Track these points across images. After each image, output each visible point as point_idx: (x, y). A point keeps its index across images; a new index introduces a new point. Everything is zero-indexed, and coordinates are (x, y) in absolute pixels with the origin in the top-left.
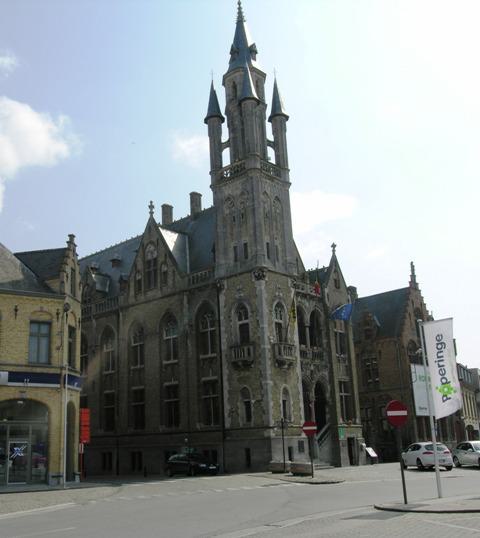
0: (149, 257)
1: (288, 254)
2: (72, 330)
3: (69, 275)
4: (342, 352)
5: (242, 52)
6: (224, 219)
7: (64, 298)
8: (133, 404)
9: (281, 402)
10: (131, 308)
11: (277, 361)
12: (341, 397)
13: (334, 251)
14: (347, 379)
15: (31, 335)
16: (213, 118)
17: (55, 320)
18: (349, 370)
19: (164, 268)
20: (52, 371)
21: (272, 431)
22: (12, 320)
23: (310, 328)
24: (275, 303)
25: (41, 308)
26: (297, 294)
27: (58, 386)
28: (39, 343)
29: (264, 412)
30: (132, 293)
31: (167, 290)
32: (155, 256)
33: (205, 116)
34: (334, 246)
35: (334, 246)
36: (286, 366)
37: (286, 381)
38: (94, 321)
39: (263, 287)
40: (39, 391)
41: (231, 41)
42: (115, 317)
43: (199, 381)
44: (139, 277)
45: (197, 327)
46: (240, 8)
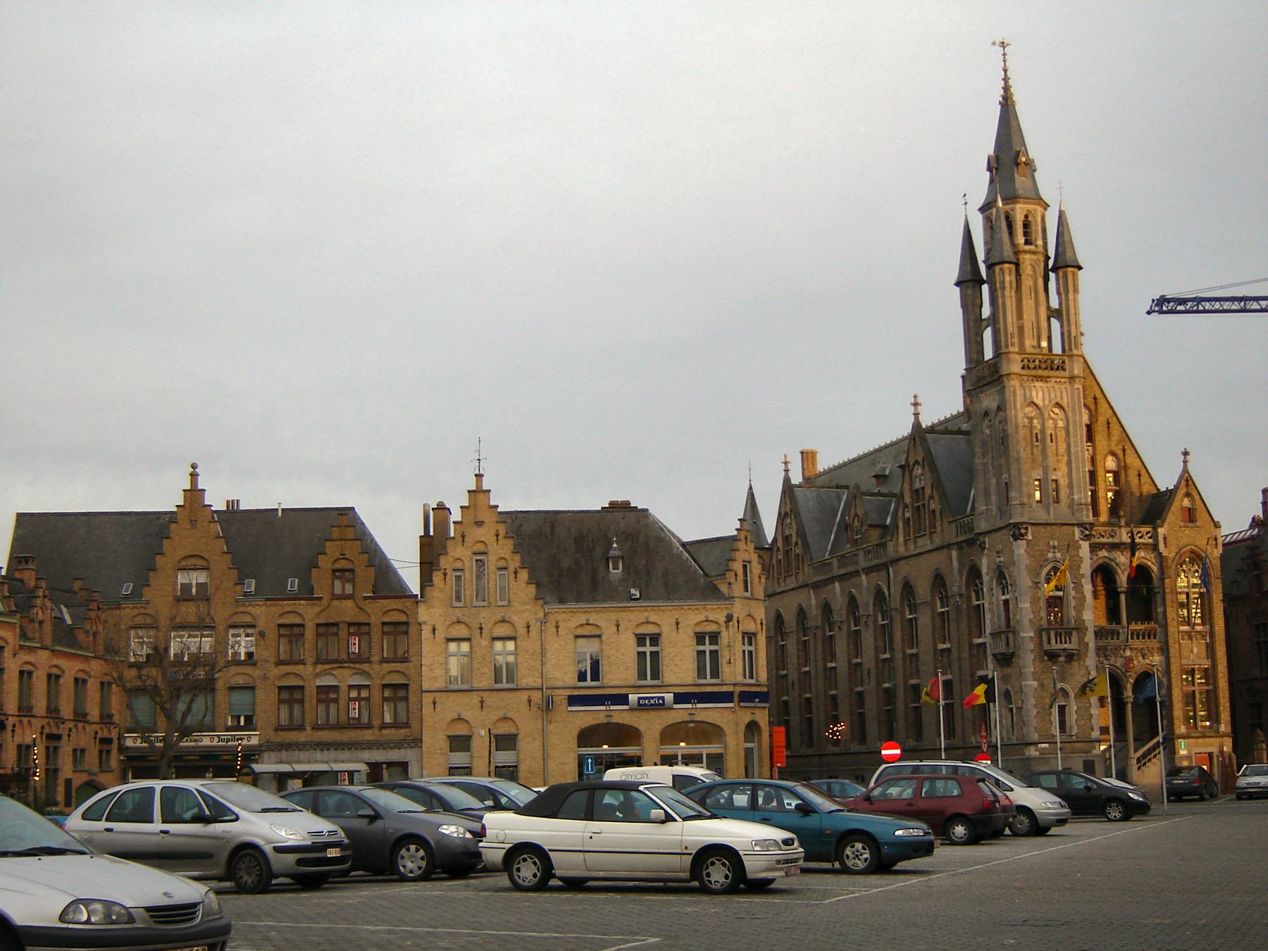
0: (917, 486)
1: (1075, 490)
4: (860, 695)
11: (1047, 653)
13: (1185, 462)
14: (1206, 664)
17: (723, 629)
18: (1211, 650)
19: (933, 506)
20: (724, 689)
21: (1032, 748)
22: (674, 634)
26: (1094, 548)
27: (731, 705)
30: (901, 539)
31: (938, 541)
33: (980, 204)
34: (1186, 454)
35: (1186, 454)
38: (864, 577)
39: (1022, 551)
40: (710, 712)
41: (987, 145)
43: (972, 675)
45: (969, 597)
46: (1006, 79)
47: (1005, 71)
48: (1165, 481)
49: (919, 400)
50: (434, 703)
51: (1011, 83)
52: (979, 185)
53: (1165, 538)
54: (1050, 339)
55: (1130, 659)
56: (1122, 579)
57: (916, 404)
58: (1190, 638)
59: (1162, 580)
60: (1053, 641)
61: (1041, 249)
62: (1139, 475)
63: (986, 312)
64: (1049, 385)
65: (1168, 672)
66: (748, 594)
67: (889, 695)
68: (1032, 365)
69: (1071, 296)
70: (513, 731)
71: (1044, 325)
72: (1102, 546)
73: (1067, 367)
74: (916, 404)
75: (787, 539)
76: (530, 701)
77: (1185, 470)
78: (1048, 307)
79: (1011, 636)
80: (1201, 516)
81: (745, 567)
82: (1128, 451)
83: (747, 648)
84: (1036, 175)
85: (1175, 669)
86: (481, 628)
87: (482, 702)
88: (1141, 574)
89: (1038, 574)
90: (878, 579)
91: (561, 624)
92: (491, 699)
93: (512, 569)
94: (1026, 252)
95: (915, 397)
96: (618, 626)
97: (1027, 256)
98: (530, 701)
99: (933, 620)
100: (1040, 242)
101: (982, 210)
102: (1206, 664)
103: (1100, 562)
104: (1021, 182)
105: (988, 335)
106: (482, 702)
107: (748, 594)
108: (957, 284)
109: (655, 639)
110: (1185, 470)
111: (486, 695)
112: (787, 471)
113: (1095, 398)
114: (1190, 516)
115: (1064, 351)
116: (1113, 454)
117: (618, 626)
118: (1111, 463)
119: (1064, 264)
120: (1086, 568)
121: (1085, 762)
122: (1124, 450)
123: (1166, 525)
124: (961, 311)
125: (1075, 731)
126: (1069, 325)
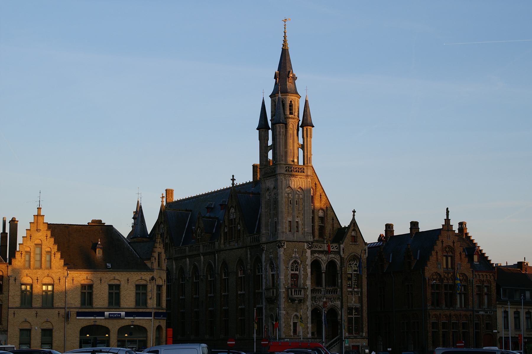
0: (231, 217)
1: (306, 227)
2: (159, 287)
3: (157, 258)
5: (284, 74)
7: (153, 271)
9: (292, 324)
11: (290, 299)
13: (354, 215)
15: (136, 293)
16: (263, 127)
17: (149, 283)
19: (239, 228)
20: (148, 310)
22: (126, 285)
24: (291, 262)
25: (141, 278)
26: (313, 253)
28: (215, 257)
30: (222, 241)
34: (354, 212)
35: (354, 212)
36: (296, 302)
37: (297, 311)
38: (202, 257)
39: (282, 253)
41: (275, 68)
44: (226, 230)
46: (285, 37)
47: (285, 33)
50: (14, 314)
51: (287, 38)
52: (270, 86)
53: (343, 249)
56: (324, 266)
60: (293, 294)
61: (296, 117)
62: (333, 219)
63: (270, 143)
64: (297, 179)
69: (309, 139)
70: (51, 327)
73: (305, 171)
76: (59, 314)
77: (354, 219)
81: (159, 255)
86: (37, 280)
87: (37, 314)
88: (331, 264)
89: (288, 264)
91: (75, 279)
92: (41, 312)
93: (53, 252)
95: (233, 176)
96: (101, 280)
98: (59, 314)
100: (296, 114)
104: (289, 85)
106: (37, 314)
109: (118, 287)
110: (354, 219)
111: (39, 310)
113: (316, 184)
115: (304, 164)
117: (101, 280)
120: (309, 262)
123: (344, 244)
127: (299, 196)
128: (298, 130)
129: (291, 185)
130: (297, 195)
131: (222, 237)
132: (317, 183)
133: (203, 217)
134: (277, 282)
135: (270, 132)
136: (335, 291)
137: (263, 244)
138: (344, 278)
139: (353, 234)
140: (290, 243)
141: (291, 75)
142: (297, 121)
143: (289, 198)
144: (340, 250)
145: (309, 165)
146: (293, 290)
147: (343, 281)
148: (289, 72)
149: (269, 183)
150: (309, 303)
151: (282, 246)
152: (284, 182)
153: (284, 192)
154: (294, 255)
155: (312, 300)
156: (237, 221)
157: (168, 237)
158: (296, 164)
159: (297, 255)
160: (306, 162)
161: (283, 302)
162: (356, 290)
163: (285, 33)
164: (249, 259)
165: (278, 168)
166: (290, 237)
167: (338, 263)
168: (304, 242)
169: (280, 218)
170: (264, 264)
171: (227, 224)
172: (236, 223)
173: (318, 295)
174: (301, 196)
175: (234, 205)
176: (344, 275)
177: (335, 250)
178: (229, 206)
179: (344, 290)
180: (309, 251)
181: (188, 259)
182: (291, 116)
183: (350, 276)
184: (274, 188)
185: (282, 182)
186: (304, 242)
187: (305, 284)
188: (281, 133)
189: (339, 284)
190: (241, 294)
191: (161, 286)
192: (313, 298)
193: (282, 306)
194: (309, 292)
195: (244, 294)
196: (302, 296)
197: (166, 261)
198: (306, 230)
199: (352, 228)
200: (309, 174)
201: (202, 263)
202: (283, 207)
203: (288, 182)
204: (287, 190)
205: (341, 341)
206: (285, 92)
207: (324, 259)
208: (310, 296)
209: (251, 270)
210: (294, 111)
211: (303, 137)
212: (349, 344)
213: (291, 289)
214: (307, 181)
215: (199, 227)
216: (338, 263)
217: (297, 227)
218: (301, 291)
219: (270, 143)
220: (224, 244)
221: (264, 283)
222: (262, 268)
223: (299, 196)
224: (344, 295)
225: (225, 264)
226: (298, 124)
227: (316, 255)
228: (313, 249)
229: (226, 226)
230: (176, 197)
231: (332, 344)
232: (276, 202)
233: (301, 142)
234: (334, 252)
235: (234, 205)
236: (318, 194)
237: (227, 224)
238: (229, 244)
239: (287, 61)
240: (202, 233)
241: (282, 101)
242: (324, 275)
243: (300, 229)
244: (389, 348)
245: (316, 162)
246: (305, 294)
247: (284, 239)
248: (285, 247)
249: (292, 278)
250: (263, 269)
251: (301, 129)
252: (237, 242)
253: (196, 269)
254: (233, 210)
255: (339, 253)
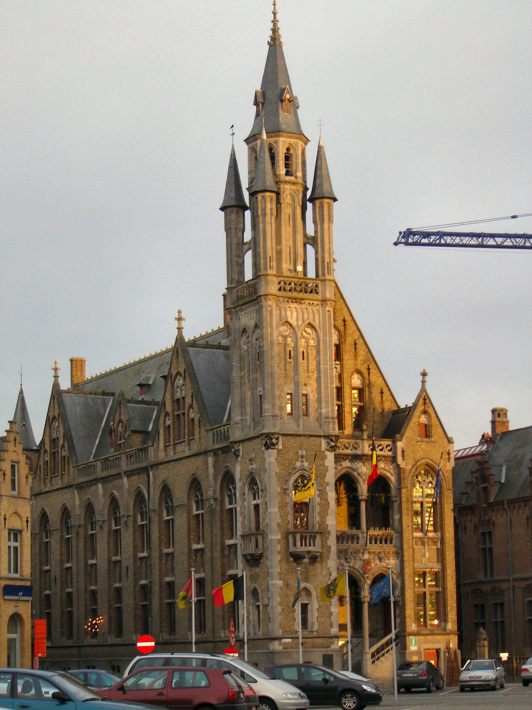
0: (178, 395)
1: (323, 405)
6: (241, 357)
8: (166, 601)
10: (161, 467)
11: (292, 555)
12: (9, 547)
13: (423, 382)
14: (437, 567)
16: (234, 206)
19: (192, 415)
23: (367, 501)
26: (339, 458)
28: (148, 476)
29: (269, 619)
30: (162, 445)
32: (183, 395)
33: (246, 136)
34: (424, 374)
35: (424, 374)
36: (306, 560)
38: (125, 479)
39: (273, 459)
42: (145, 476)
44: (168, 422)
45: (222, 501)
46: (275, 22)
47: (275, 14)
48: (405, 399)
49: (183, 315)
51: (279, 25)
52: (246, 119)
53: (403, 452)
54: (305, 264)
55: (368, 562)
56: (363, 489)
57: (179, 319)
58: (423, 543)
59: (399, 489)
61: (300, 180)
62: (382, 393)
63: (248, 236)
64: (304, 306)
65: (402, 574)
66: (15, 493)
67: (145, 591)
68: (288, 288)
69: (326, 225)
71: (300, 250)
72: (345, 457)
73: (320, 290)
74: (179, 319)
75: (54, 442)
77: (423, 390)
78: (305, 235)
79: (260, 538)
80: (436, 431)
81: (13, 467)
82: (373, 370)
83: (13, 544)
84: (299, 111)
85: (408, 572)
88: (379, 483)
89: (287, 481)
90: (138, 481)
94: (286, 182)
95: (179, 312)
97: (288, 186)
99: (189, 522)
100: (300, 174)
101: (247, 141)
102: (437, 567)
103: (344, 471)
104: (284, 117)
105: (248, 258)
107: (15, 493)
108: (222, 209)
110: (423, 390)
112: (56, 377)
113: (344, 321)
114: (426, 432)
115: (317, 275)
116: (359, 372)
118: (356, 381)
119: (319, 196)
120: (331, 477)
121: (324, 656)
122: (369, 369)
123: (404, 439)
124: (223, 235)
125: (316, 628)
126: (323, 251)
127: (307, 342)
128: (304, 209)
129: (290, 320)
130: (303, 340)
131: (162, 437)
132: (348, 318)
133: (129, 401)
134: (264, 519)
135: (248, 214)
136: (386, 540)
137: (236, 442)
138: (404, 511)
139: (423, 419)
140: (292, 440)
141: (288, 96)
142: (301, 189)
143: (286, 345)
144: (395, 453)
145: (328, 277)
146: (298, 537)
147: (405, 518)
148: (283, 90)
149: (247, 319)
150: (332, 563)
151: (273, 444)
152: (275, 312)
153: (275, 334)
154: (298, 464)
155: (339, 558)
156: (188, 401)
157: (66, 445)
158: (301, 275)
159: (306, 464)
160: (320, 273)
161: (275, 561)
162: (431, 535)
163: (275, 14)
164: (211, 477)
165: (263, 283)
166: (291, 427)
167: (393, 479)
168: (320, 436)
169: (268, 386)
170: (238, 484)
171: (169, 408)
172: (187, 405)
173: (351, 546)
174: (312, 343)
175: (182, 370)
176: (404, 506)
177: (386, 453)
178: (174, 375)
179: (406, 535)
180: (330, 456)
181: (100, 485)
182: (288, 178)
183: (417, 507)
184: (256, 326)
185: (271, 312)
186: (320, 436)
187: (323, 523)
188: (268, 211)
189: (396, 524)
190: (197, 551)
191: (21, 531)
192: (342, 554)
193: (276, 569)
194: (332, 541)
195: (202, 550)
196: (315, 548)
197: (30, 480)
198: (324, 411)
199: (420, 408)
200: (328, 296)
201: (125, 491)
202: (275, 363)
203: (283, 313)
204: (282, 328)
205: (401, 640)
206: (275, 132)
207: (364, 470)
208: (334, 549)
209: (215, 499)
210: (294, 168)
211: (315, 222)
212: (419, 648)
213: (294, 534)
214: (324, 312)
215: (120, 421)
216: (393, 479)
217: (306, 404)
218: (315, 538)
219: (248, 236)
220: (165, 451)
221: (239, 525)
222: (235, 494)
223: (307, 342)
224: (405, 546)
225: (166, 491)
226: (305, 195)
227: (347, 464)
228: (340, 451)
229: (167, 414)
230: (92, 371)
231: (383, 647)
232: (260, 355)
233: (310, 231)
234: (384, 456)
235: (182, 370)
236: (349, 341)
237: (169, 408)
238: (174, 449)
239: (280, 68)
240: (125, 431)
241: (271, 149)
242: (363, 505)
243: (311, 410)
244: (504, 652)
245: (341, 274)
246: (324, 544)
247: (276, 430)
248: (280, 447)
249: (296, 512)
250: (238, 495)
251: (309, 205)
252: (189, 444)
253: (114, 503)
254: (180, 381)
255: (394, 459)
